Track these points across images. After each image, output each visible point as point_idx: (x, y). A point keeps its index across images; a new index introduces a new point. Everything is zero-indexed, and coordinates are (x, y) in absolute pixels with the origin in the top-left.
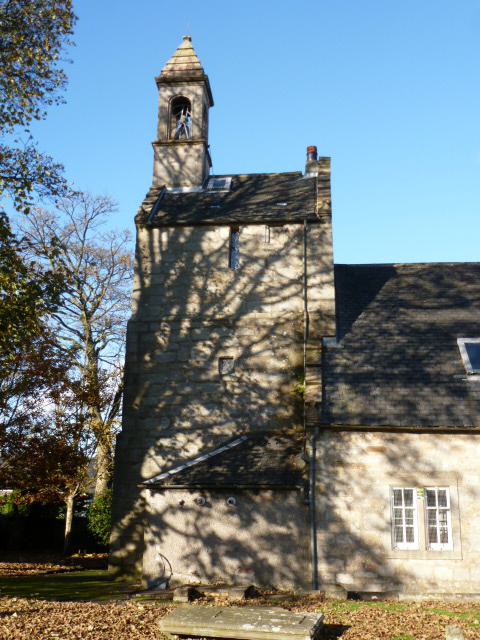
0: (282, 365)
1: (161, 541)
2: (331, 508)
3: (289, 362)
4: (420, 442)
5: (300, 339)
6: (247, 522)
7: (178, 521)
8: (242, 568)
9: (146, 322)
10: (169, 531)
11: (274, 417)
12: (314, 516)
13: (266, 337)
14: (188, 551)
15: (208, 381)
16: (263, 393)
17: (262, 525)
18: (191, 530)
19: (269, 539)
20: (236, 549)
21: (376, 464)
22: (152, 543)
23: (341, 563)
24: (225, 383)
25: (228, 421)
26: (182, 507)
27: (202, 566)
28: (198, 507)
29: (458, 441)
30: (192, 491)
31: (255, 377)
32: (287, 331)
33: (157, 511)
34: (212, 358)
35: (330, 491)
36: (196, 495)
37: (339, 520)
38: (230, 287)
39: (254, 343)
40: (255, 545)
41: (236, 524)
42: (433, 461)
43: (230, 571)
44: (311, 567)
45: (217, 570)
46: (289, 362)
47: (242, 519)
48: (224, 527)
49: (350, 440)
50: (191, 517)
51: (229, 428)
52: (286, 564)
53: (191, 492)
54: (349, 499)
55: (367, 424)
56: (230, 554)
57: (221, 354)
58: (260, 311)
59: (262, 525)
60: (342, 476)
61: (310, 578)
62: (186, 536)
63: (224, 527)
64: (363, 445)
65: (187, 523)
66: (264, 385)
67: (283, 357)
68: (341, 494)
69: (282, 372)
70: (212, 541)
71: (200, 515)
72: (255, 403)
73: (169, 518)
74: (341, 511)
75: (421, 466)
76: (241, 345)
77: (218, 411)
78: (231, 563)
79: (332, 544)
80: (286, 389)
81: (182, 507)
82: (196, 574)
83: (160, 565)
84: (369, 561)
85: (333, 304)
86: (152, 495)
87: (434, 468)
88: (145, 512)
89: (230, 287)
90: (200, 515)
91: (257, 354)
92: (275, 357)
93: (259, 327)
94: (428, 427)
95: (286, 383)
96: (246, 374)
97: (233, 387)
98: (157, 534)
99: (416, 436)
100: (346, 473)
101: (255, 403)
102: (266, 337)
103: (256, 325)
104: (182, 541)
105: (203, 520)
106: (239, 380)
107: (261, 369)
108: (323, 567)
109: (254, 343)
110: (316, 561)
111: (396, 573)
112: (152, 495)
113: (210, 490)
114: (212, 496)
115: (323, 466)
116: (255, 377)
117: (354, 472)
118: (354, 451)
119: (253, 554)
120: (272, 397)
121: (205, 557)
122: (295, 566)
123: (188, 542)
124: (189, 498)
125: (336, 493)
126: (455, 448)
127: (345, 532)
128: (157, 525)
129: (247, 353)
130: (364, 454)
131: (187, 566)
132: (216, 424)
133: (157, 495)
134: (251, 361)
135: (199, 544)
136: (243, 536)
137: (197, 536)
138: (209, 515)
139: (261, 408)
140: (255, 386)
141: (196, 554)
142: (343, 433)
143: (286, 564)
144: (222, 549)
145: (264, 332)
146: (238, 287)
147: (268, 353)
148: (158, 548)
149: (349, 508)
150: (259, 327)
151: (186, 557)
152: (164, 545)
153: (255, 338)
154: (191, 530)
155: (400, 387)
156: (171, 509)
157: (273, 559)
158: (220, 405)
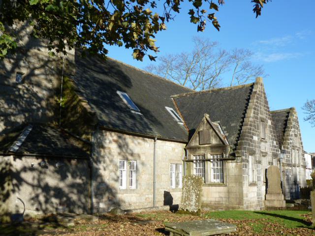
0: (49, 85)
1: (19, 189)
2: (98, 169)
3: (53, 85)
4: (128, 139)
5: (59, 73)
6: (63, 178)
7: (28, 176)
8: (61, 204)
9: (186, 79)
10: (23, 183)
11: (44, 114)
12: (92, 174)
13: (42, 67)
14: (33, 195)
15: (9, 85)
16: (40, 100)
17: (70, 179)
18: (36, 182)
19: (72, 186)
20: (59, 193)
21: (114, 147)
22: (14, 191)
23: (100, 197)
24: (19, 90)
25: (19, 114)
26: (32, 169)
27: (40, 204)
28: (40, 168)
29: (140, 140)
30: (37, 158)
31: (35, 89)
32: (53, 66)
33: (17, 170)
34: (12, 71)
35: (98, 161)
36: (40, 161)
37: (100, 176)
38: (23, 28)
39: (35, 68)
40: (66, 190)
41: (59, 179)
42: (132, 149)
43: (55, 206)
44: (89, 201)
45: (49, 206)
46: (53, 85)
47: (62, 176)
48: (52, 180)
49: (106, 135)
50: (35, 174)
51: (21, 118)
52: (80, 200)
53: (37, 159)
54: (105, 165)
55: (113, 129)
56: (56, 196)
57: (17, 70)
58: (39, 50)
59: (70, 179)
60: (102, 153)
61: (89, 206)
62: (33, 186)
63: (52, 180)
64: (111, 138)
65: (34, 178)
66: (40, 95)
67: (50, 81)
68: (102, 162)
69: (49, 90)
70: (46, 189)
71: (41, 172)
72: (35, 105)
73: (23, 175)
74: (102, 172)
75: (129, 151)
76: (29, 67)
77: (13, 106)
78: (55, 201)
79: (98, 188)
80: (51, 100)
81: (32, 169)
82: (37, 210)
83: (17, 206)
84: (110, 196)
85: (74, 58)
86: (15, 160)
87: (132, 152)
88: (10, 170)
89: (23, 28)
90: (41, 172)
91: (37, 75)
92: (46, 79)
93: (40, 60)
94: (134, 134)
95: (52, 97)
96: (31, 87)
97: (24, 93)
98: (17, 186)
99: (128, 136)
100: (104, 152)
101: (35, 105)
102: (42, 67)
103: (38, 58)
104: (30, 189)
105: (42, 176)
106: (27, 90)
107: (38, 85)
108: (94, 200)
109: (35, 68)
110: (91, 197)
111: (119, 201)
112: (15, 160)
113: (48, 158)
114: (48, 162)
115: (96, 147)
116: (35, 89)
117: (107, 151)
118: (107, 141)
119: (66, 196)
120: (44, 103)
121: (42, 198)
122: (83, 200)
123: (34, 189)
124: (34, 162)
125: (100, 162)
126: (139, 143)
127: (103, 182)
128: (17, 179)
129: (32, 74)
130: (110, 140)
131: (33, 205)
132: (13, 114)
133: (18, 160)
134: (34, 79)
135: (40, 191)
136: (62, 185)
137: (39, 186)
138: (45, 173)
139: (38, 109)
140: (35, 95)
141: (37, 196)
142: (104, 131)
143: (80, 200)
144: (52, 193)
145: (42, 63)
146: (28, 30)
147: (43, 77)
148: (17, 195)
149: (105, 169)
150: (40, 60)
151: (33, 199)
152: (20, 192)
153: (37, 65)
154: (36, 182)
155: (52, 103)
156: (25, 169)
157: (74, 197)
158: (16, 103)
